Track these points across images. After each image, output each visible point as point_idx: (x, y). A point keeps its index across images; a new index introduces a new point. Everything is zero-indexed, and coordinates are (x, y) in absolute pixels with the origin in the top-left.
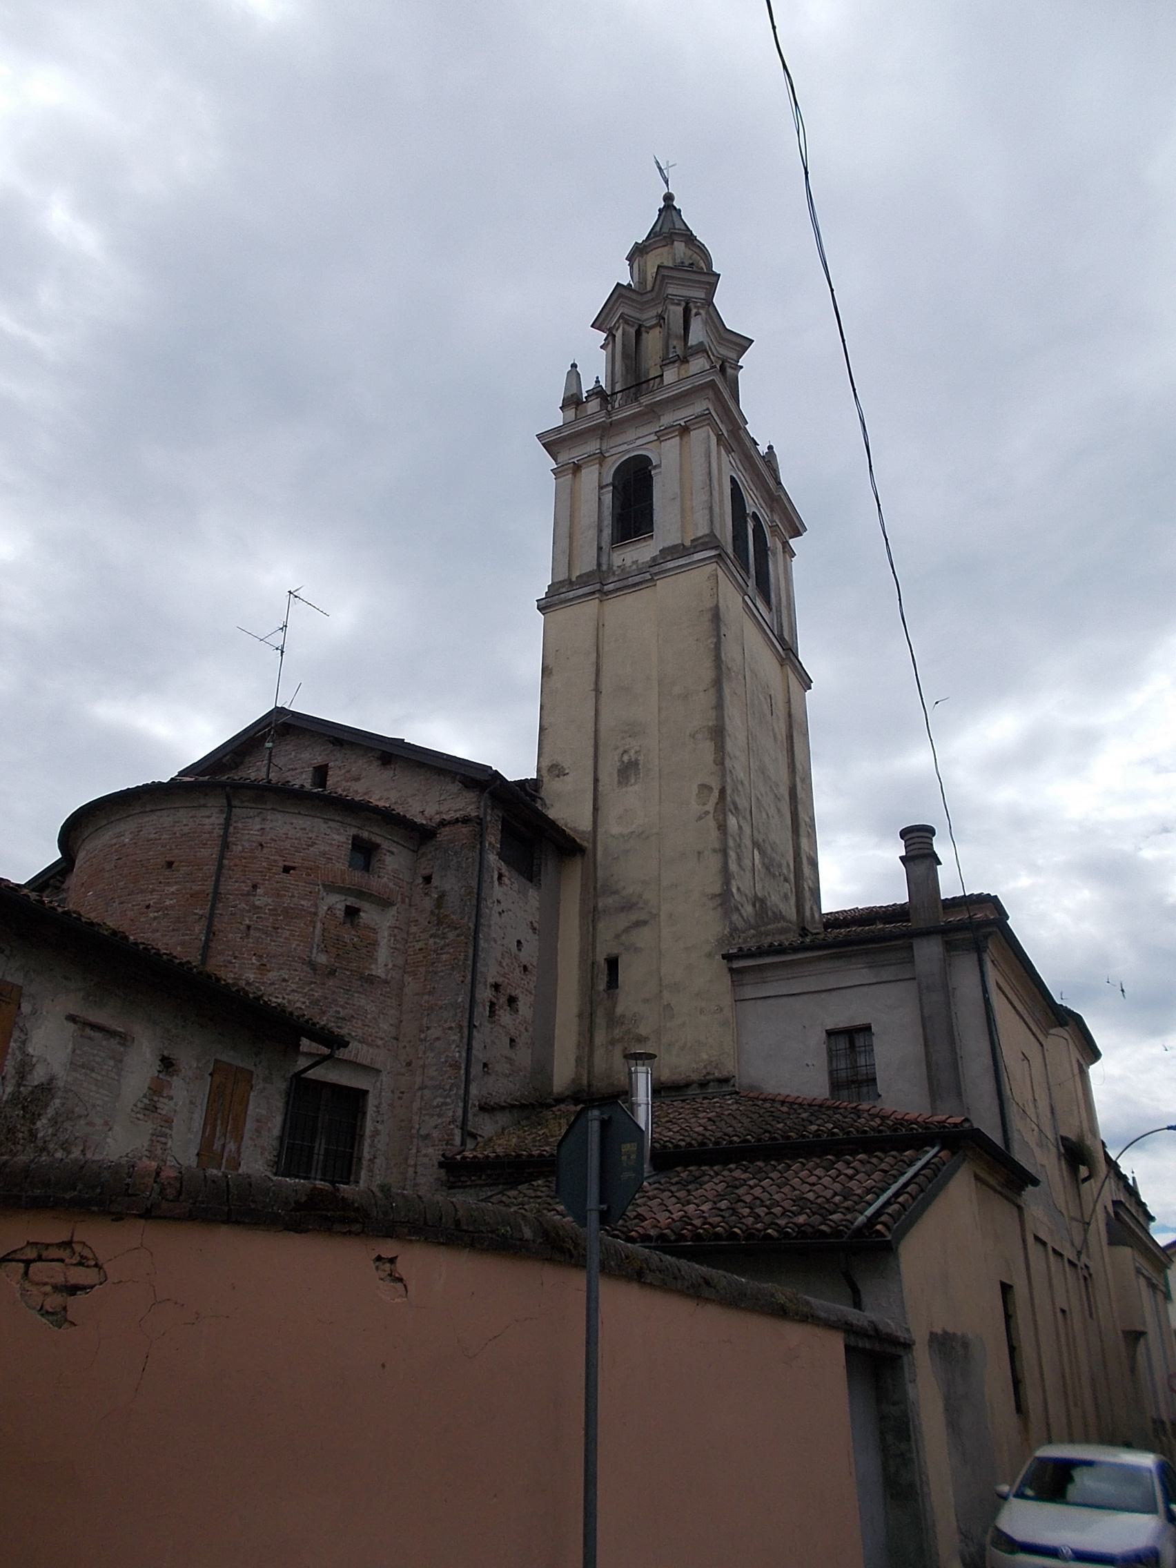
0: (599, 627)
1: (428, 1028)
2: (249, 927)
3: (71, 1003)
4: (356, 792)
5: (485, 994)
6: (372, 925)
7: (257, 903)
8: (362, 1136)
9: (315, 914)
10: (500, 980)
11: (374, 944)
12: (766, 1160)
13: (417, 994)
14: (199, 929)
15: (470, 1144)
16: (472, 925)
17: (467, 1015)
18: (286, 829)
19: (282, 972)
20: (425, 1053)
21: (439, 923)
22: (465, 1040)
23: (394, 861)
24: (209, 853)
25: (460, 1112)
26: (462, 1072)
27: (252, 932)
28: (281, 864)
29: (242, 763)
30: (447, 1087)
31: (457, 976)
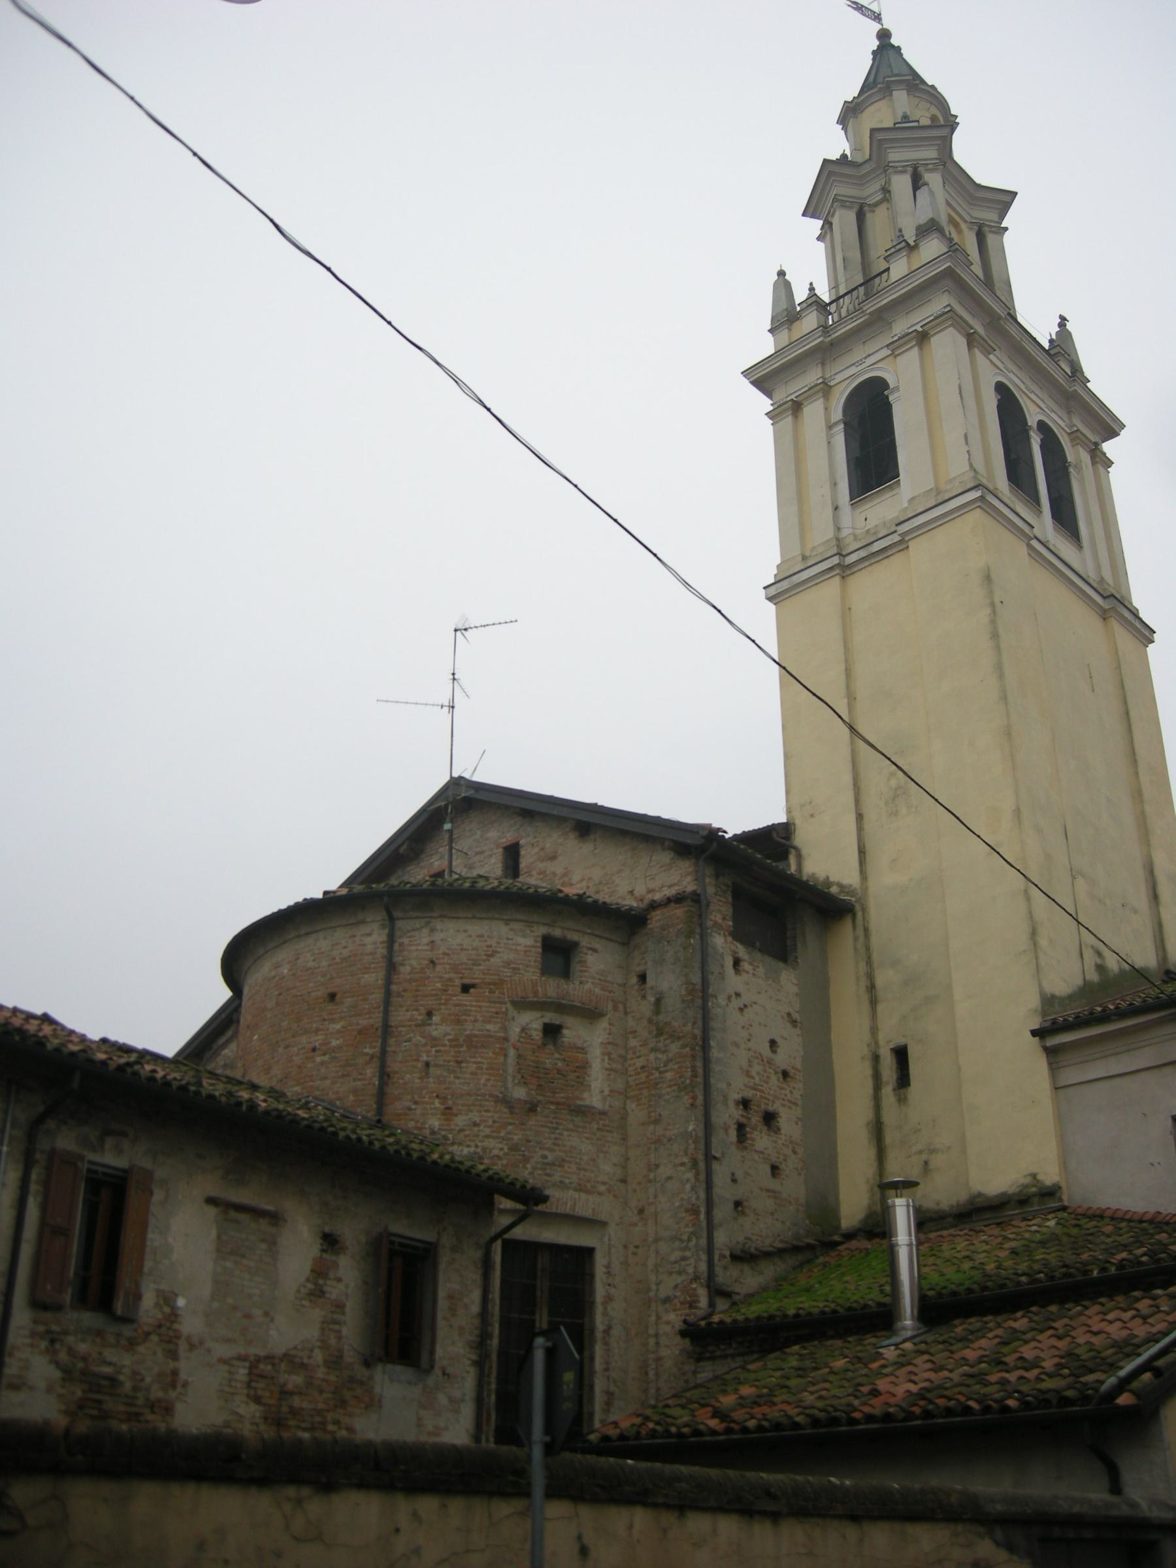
0: (846, 612)
1: (657, 1166)
2: (427, 1064)
3: (209, 1183)
4: (554, 874)
5: (727, 1115)
6: (579, 1043)
7: (435, 1033)
8: (593, 1303)
9: (506, 1039)
10: (749, 1094)
11: (584, 1066)
12: (1062, 1302)
13: (643, 1124)
14: (371, 1072)
15: (722, 1304)
16: (698, 1032)
17: (702, 1146)
18: (457, 938)
19: (471, 1115)
20: (656, 1197)
21: (660, 1032)
22: (702, 1177)
23: (598, 960)
24: (374, 978)
25: (703, 1267)
26: (702, 1216)
27: (432, 1069)
28: (458, 982)
29: (422, 851)
30: (685, 1237)
31: (686, 1100)
